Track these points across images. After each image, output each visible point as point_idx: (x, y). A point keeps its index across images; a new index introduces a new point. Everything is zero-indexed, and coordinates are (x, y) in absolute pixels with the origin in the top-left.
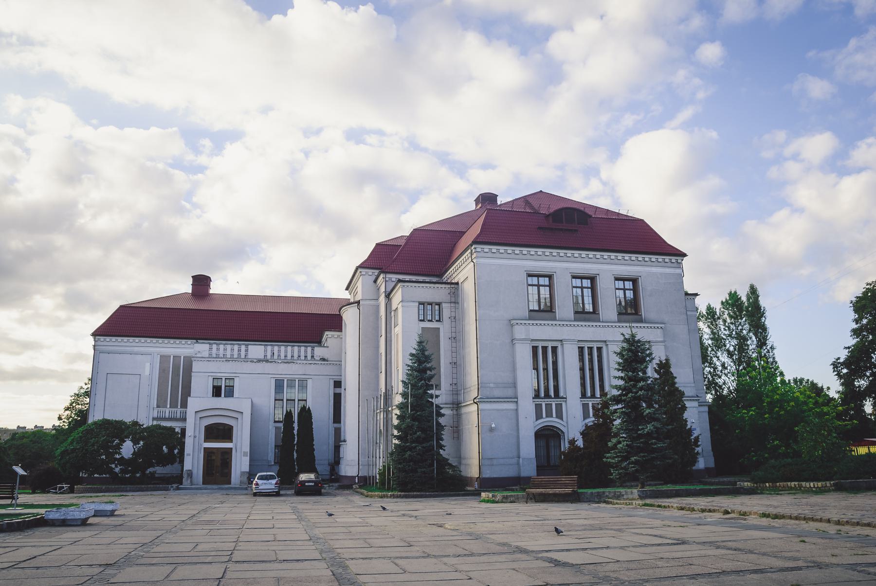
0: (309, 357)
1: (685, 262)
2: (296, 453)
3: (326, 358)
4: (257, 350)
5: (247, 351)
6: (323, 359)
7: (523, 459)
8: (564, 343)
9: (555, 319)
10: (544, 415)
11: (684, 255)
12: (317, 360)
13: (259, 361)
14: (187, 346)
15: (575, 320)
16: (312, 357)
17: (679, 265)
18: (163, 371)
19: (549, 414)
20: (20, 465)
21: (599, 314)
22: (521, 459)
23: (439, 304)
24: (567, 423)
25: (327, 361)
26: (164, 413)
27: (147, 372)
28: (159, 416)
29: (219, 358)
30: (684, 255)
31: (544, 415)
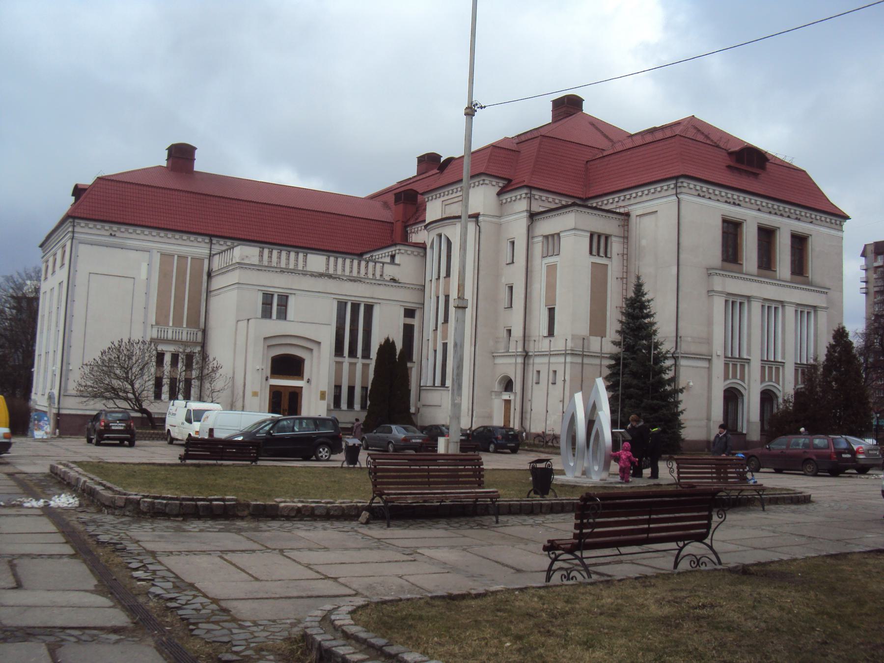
0: (378, 277)
1: (847, 224)
2: (370, 400)
3: (397, 279)
4: (317, 262)
5: (305, 261)
6: (393, 280)
7: (714, 422)
8: (786, 304)
9: (741, 273)
10: (730, 376)
11: (846, 218)
12: (386, 281)
13: (321, 275)
14: (195, 244)
15: (758, 276)
16: (381, 275)
17: (840, 228)
18: (164, 275)
19: (734, 377)
20: (802, 429)
21: (775, 271)
22: (712, 422)
23: (607, 237)
24: (749, 385)
25: (400, 283)
26: (166, 332)
27: (144, 275)
28: (189, 339)
29: (271, 267)
30: (846, 218)
31: (730, 376)
